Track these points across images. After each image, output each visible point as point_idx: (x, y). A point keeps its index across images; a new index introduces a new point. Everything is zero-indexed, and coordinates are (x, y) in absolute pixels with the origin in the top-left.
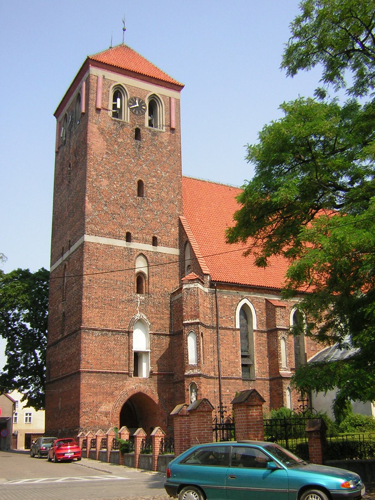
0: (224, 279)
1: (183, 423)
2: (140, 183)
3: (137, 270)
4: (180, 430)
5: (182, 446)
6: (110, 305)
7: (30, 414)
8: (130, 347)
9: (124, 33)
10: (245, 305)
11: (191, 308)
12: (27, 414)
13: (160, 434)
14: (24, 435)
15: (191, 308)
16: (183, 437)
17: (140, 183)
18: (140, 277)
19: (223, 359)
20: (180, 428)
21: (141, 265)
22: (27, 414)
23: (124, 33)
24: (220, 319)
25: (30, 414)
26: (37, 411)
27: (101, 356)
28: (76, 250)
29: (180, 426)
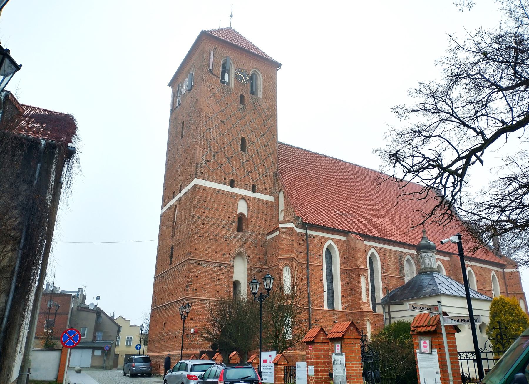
0: (313, 221)
1: (318, 351)
2: (243, 140)
3: (239, 212)
4: (316, 359)
5: (318, 378)
6: (214, 240)
7: (131, 338)
8: (230, 275)
9: (231, 19)
10: (330, 245)
11: (286, 245)
12: (128, 338)
13: (283, 361)
14: (280, 62)
15: (286, 245)
16: (319, 367)
17: (243, 140)
18: (241, 218)
19: (312, 292)
20: (324, 356)
21: (242, 208)
22: (128, 338)
23: (231, 19)
24: (309, 256)
25: (131, 338)
26: (169, 85)
27: (205, 284)
28: (186, 193)
29: (316, 354)
